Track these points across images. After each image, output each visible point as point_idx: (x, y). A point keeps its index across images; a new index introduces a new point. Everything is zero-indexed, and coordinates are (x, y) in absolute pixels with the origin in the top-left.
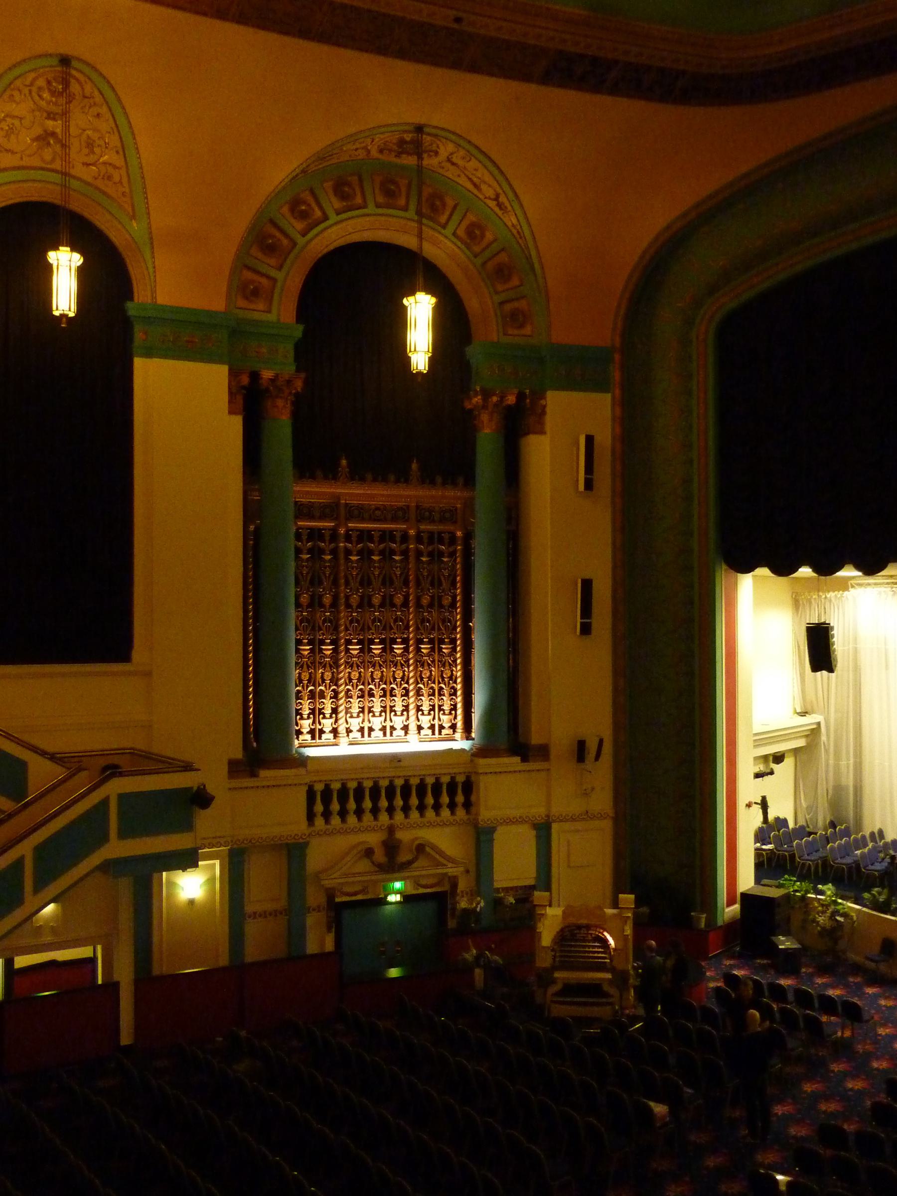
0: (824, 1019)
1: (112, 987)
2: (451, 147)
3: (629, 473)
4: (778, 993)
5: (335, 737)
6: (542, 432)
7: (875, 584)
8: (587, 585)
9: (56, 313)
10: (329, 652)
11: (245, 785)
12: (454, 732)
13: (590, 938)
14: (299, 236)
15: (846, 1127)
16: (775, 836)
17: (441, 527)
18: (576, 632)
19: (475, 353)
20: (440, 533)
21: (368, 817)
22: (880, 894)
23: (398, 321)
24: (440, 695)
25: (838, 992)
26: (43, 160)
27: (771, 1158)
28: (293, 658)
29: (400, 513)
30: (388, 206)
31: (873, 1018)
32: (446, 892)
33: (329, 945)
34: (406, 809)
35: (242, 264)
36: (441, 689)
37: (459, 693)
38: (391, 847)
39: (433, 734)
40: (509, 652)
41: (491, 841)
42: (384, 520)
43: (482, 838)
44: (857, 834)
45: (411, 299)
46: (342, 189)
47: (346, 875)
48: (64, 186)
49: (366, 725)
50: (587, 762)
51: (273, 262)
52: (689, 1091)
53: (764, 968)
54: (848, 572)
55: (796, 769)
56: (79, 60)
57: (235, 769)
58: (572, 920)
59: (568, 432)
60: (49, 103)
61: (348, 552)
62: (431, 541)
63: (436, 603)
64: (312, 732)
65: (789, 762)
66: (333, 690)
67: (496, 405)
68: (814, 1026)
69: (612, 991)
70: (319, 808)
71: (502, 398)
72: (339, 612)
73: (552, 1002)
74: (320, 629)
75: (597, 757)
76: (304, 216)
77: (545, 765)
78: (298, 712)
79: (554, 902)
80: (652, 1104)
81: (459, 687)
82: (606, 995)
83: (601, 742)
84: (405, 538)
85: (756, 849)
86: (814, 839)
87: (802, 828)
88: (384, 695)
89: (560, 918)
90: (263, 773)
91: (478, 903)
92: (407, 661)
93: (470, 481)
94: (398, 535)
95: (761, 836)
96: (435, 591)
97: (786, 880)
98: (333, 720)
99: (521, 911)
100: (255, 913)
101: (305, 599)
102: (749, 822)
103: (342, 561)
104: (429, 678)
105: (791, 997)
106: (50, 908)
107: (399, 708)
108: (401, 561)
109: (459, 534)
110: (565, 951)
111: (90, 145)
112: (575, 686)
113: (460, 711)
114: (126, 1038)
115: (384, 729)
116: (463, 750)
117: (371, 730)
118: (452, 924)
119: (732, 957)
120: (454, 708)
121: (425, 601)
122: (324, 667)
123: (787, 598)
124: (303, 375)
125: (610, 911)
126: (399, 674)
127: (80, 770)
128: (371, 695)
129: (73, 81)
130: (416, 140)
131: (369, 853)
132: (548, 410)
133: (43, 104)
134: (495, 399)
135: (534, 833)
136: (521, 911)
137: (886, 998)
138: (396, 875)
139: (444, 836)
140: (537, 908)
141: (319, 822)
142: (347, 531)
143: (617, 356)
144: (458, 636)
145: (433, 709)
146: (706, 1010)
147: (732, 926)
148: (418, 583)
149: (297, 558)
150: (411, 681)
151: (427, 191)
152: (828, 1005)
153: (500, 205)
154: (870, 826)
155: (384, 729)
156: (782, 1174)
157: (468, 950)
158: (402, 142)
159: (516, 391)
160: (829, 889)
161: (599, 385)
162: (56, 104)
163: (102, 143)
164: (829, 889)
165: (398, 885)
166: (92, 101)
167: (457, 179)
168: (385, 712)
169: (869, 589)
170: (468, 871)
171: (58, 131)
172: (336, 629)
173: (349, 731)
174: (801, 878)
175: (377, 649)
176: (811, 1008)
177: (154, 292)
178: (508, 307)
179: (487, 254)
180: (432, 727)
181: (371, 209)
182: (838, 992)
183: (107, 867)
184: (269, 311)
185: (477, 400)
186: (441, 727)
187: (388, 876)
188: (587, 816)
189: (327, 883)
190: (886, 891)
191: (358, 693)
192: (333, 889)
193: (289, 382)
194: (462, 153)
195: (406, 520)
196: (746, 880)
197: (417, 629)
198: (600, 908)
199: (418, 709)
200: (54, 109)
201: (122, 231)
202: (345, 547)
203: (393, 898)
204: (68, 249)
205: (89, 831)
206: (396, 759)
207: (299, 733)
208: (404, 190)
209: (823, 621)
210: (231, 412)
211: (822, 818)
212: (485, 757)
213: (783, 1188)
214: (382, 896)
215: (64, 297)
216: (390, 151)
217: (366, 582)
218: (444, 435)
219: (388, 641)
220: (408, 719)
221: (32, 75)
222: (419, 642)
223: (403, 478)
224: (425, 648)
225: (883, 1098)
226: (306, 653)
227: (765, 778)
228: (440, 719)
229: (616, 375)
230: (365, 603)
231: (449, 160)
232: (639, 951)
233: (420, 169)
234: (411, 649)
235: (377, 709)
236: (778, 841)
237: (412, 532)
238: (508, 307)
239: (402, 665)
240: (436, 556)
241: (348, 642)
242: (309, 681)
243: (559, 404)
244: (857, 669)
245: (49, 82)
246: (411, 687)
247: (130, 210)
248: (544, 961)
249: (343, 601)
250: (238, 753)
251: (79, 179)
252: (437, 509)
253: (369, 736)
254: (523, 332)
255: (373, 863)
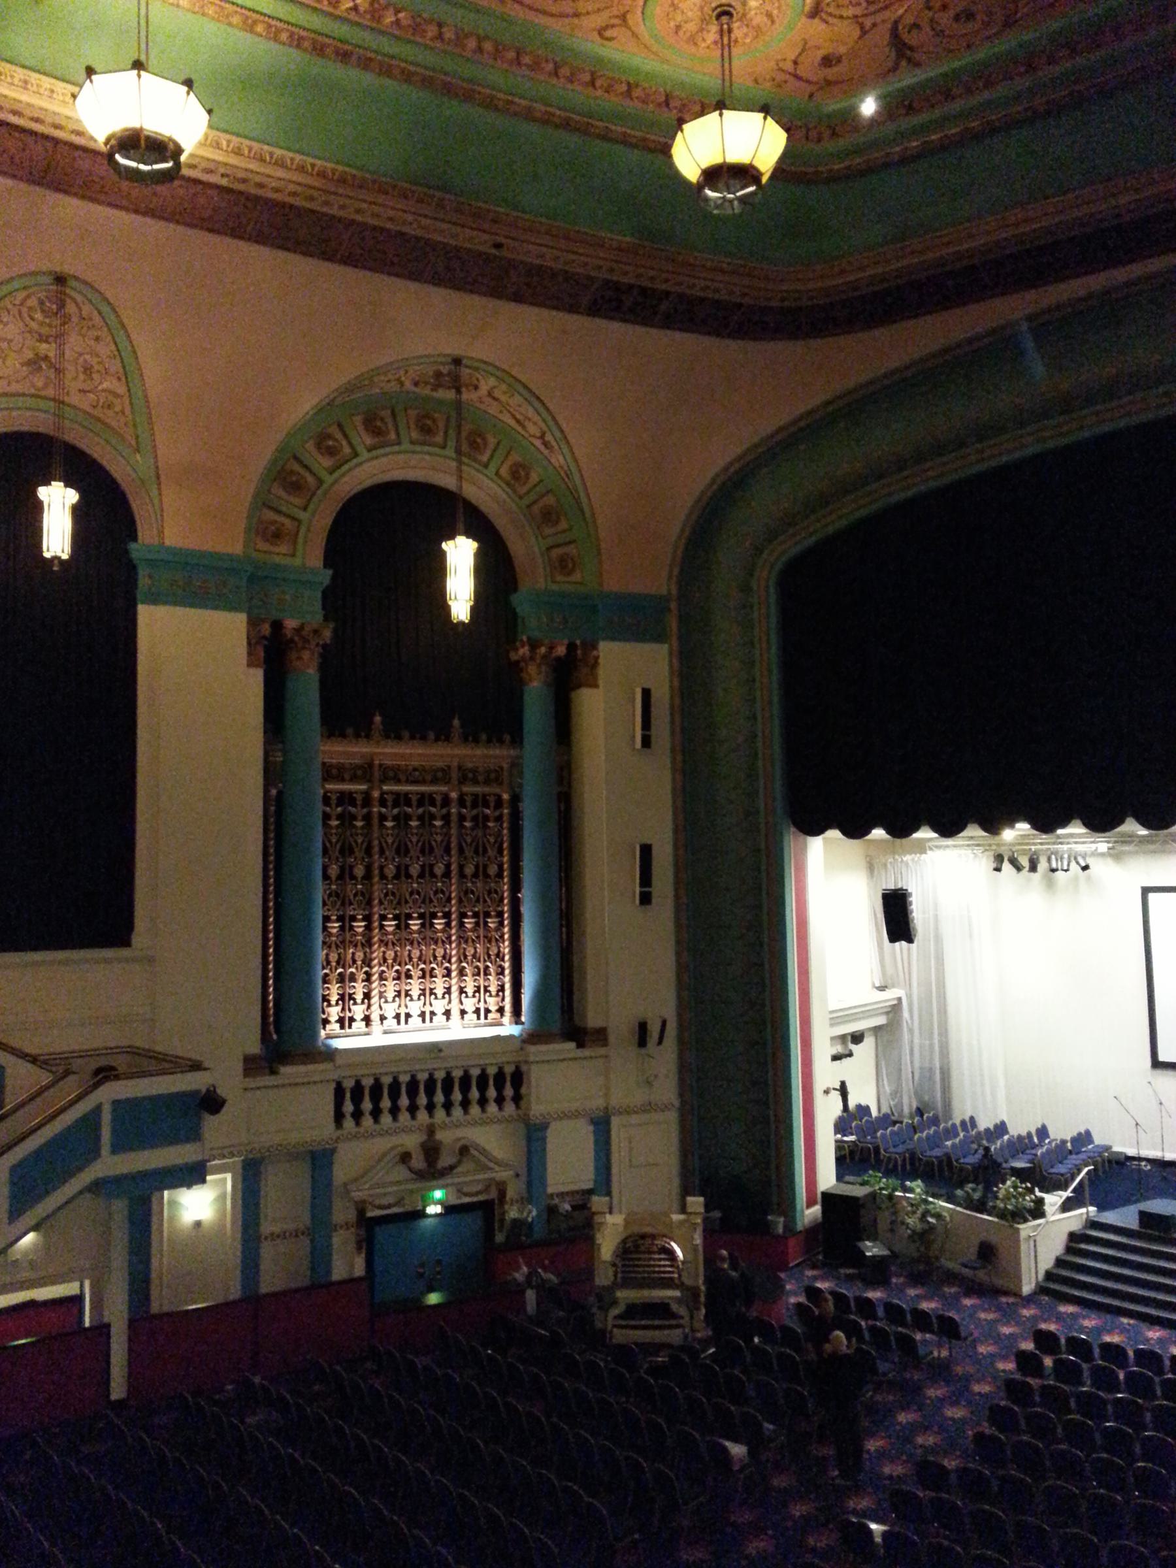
0: (918, 1336)
1: (102, 1330)
2: (492, 381)
3: (690, 731)
4: (866, 1306)
5: (368, 1025)
6: (596, 686)
7: (955, 846)
8: (646, 850)
9: (47, 555)
10: (360, 930)
11: (261, 1084)
12: (502, 1015)
13: (655, 1249)
14: (325, 473)
15: (946, 1463)
16: (857, 1126)
17: (487, 790)
18: (634, 901)
19: (521, 602)
20: (484, 796)
21: (404, 1117)
22: (974, 1190)
23: (437, 568)
24: (486, 974)
25: (933, 1305)
26: (33, 386)
27: (864, 1503)
28: (320, 937)
29: (359, 773)
30: (424, 443)
31: (972, 1334)
32: (493, 1200)
33: (359, 1270)
34: (448, 1106)
35: (262, 502)
36: (487, 967)
37: (507, 972)
38: (431, 1150)
39: (479, 1018)
40: (561, 926)
41: (544, 1139)
42: (423, 782)
43: (534, 1136)
44: (946, 1122)
45: (450, 543)
46: (372, 425)
47: (378, 1185)
48: (59, 416)
49: (403, 1011)
50: (649, 1045)
51: (297, 501)
52: (771, 1427)
53: (849, 1278)
54: (925, 834)
55: (877, 1056)
56: (76, 278)
57: (252, 1065)
58: (636, 1229)
59: (624, 681)
60: (42, 324)
61: (383, 818)
62: (475, 805)
63: (481, 872)
64: (341, 1021)
65: (869, 1042)
66: (366, 973)
67: (544, 657)
68: (907, 1345)
69: (682, 1311)
70: (348, 1107)
71: (551, 648)
72: (372, 885)
73: (615, 1326)
74: (351, 904)
75: (660, 1042)
76: (331, 452)
77: (602, 1051)
78: (325, 999)
79: (615, 1210)
80: (727, 1444)
81: (507, 965)
82: (675, 1316)
83: (664, 1023)
84: (446, 801)
85: (836, 1141)
86: (901, 1129)
87: (886, 1116)
88: (423, 977)
89: (621, 1229)
90: (285, 1070)
91: (530, 1212)
92: (449, 938)
93: (517, 739)
94: (438, 798)
95: (841, 1126)
96: (481, 858)
97: (871, 1176)
98: (365, 1006)
99: (573, 1224)
100: (272, 1234)
101: (334, 870)
102: (828, 1111)
103: (376, 828)
104: (474, 956)
105: (881, 1312)
106: (30, 1238)
107: (440, 991)
108: (442, 827)
109: (506, 796)
110: (629, 1266)
111: (88, 370)
112: (635, 961)
113: (508, 992)
114: (118, 1390)
115: (423, 1015)
116: (511, 1037)
117: (408, 1016)
118: (500, 1238)
119: (814, 1267)
120: (502, 989)
121: (469, 870)
122: (356, 946)
123: (863, 863)
124: (332, 625)
125: (677, 1217)
126: (440, 952)
127: (67, 1073)
128: (409, 976)
129: (68, 301)
130: (454, 374)
131: (405, 1157)
132: (601, 661)
133: (33, 325)
134: (543, 650)
135: (591, 1128)
136: (573, 1224)
137: (985, 1310)
138: (434, 1183)
139: (490, 1135)
140: (596, 1217)
141: (349, 1123)
142: (383, 793)
143: (673, 605)
144: (506, 909)
145: (478, 990)
146: (785, 1329)
147: (813, 1231)
148: (461, 851)
149: (325, 825)
150: (454, 960)
151: (467, 428)
152: (922, 1320)
153: (546, 444)
154: (961, 1112)
155: (423, 1015)
156: (877, 1522)
157: (518, 1269)
158: (438, 375)
159: (566, 641)
160: (918, 1186)
161: (659, 638)
162: (50, 326)
163: (100, 368)
164: (918, 1186)
165: (438, 1194)
166: (90, 324)
167: (500, 416)
168: (424, 995)
169: (948, 851)
170: (517, 1175)
171: (51, 354)
172: (369, 903)
173: (383, 1018)
174: (888, 1173)
175: (415, 925)
176: (903, 1324)
177: (161, 532)
178: (556, 552)
179: (532, 497)
180: (477, 1011)
181: (406, 446)
182: (933, 1305)
183: (96, 1187)
184: (293, 555)
185: (524, 651)
186: (487, 1011)
187: (428, 1184)
188: (648, 1107)
189: (357, 1195)
190: (980, 1187)
191: (394, 974)
192: (364, 1202)
193: (316, 632)
194: (504, 387)
195: (447, 781)
196: (827, 1178)
197: (460, 901)
198: (667, 1215)
199: (462, 991)
200: (45, 331)
201: (121, 466)
202: (380, 813)
203: (433, 1209)
204: (62, 484)
205: (79, 1144)
206: (435, 1049)
207: (326, 1022)
208: (441, 425)
209: (899, 886)
210: (250, 664)
211: (908, 1104)
212: (534, 1044)
213: (878, 1540)
214: (420, 1208)
215: (57, 536)
216: (426, 383)
217: (402, 850)
218: (488, 688)
219: (428, 915)
220: (450, 1002)
221: (24, 294)
222: (463, 915)
223: (443, 736)
224: (469, 923)
225: (987, 1429)
226: (335, 931)
227: (844, 1060)
228: (485, 1002)
229: (673, 624)
230: (402, 873)
231: (490, 394)
232: (710, 1260)
233: (458, 405)
234: (454, 923)
235: (415, 993)
236: (860, 1132)
237: (454, 795)
238: (556, 552)
239: (443, 942)
240: (480, 822)
241: (383, 918)
242: (338, 963)
243: (613, 655)
244: (938, 939)
245: (41, 303)
246: (454, 967)
247: (133, 443)
248: (603, 1278)
249: (376, 872)
250: (254, 1046)
251: (74, 407)
252: (481, 769)
253: (406, 1022)
254: (572, 578)
255: (410, 1169)
